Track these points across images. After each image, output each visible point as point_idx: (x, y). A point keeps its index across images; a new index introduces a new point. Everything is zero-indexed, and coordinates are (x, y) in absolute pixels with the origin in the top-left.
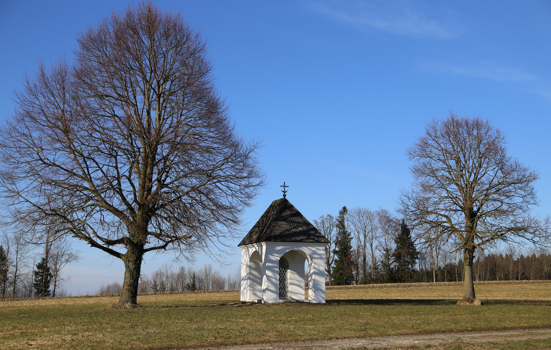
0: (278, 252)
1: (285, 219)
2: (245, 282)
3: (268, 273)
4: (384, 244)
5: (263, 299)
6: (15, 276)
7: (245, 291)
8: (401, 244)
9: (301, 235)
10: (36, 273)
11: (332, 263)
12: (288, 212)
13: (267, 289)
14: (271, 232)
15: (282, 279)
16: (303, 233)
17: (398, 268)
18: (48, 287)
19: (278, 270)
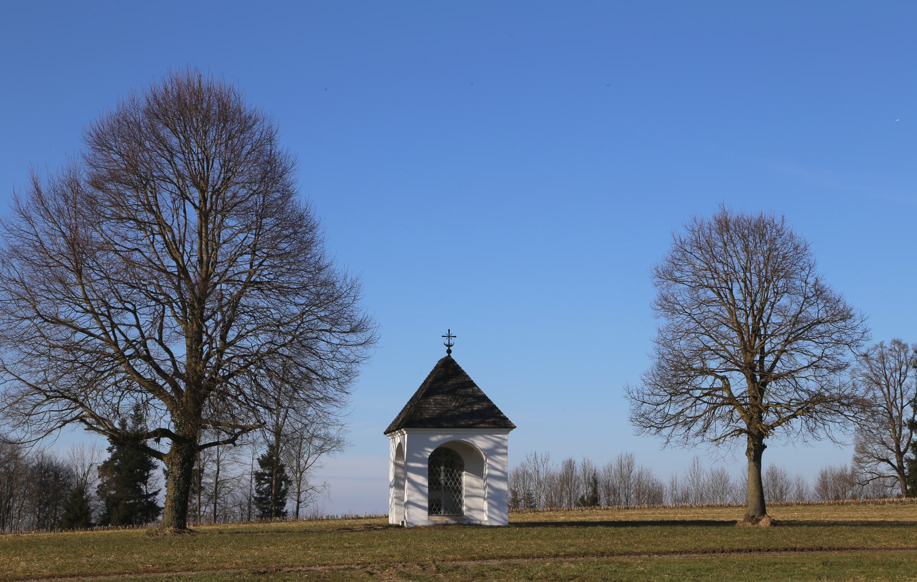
6: (217, 483)
10: (259, 477)
11: (905, 451)
18: (284, 504)
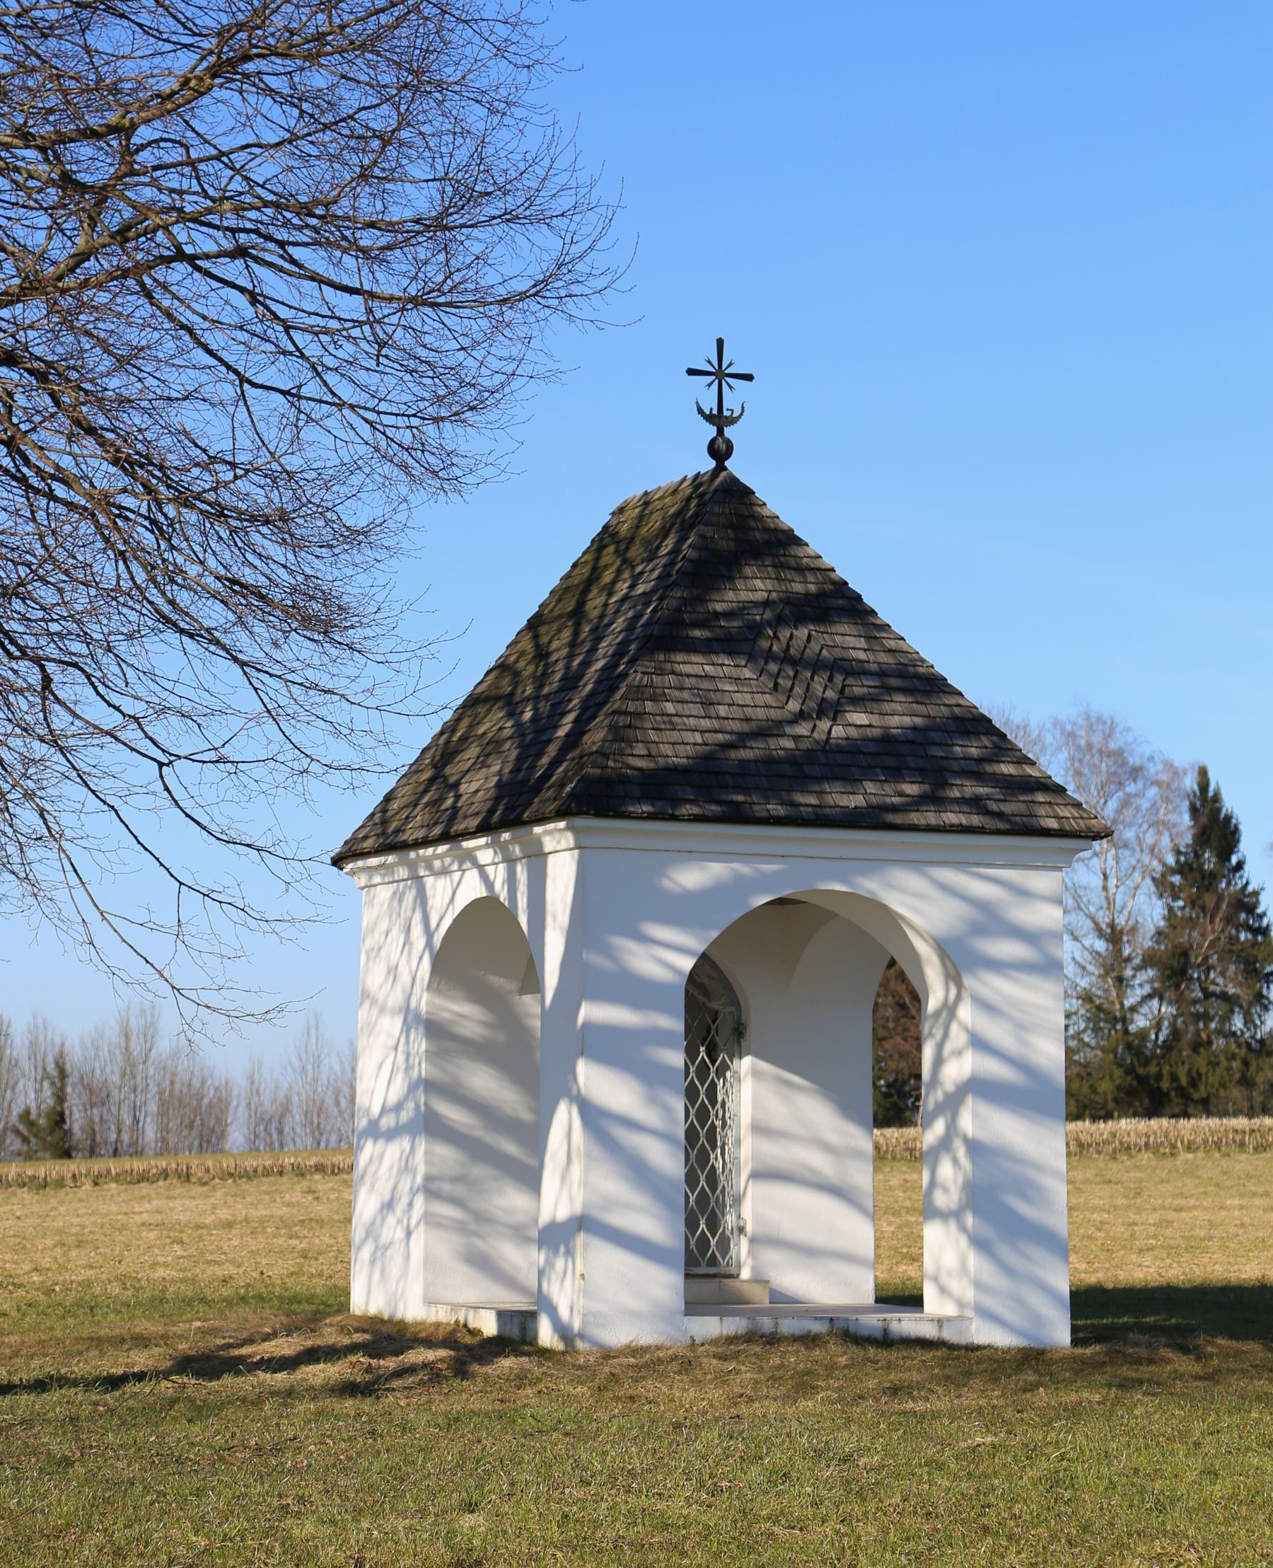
0: (680, 910)
1: (739, 640)
2: (394, 1151)
3: (597, 1081)
4: (1097, 898)
5: (544, 1303)
7: (392, 1230)
8: (1193, 903)
9: (868, 772)
12: (755, 586)
13: (583, 1223)
14: (619, 735)
15: (702, 1137)
16: (886, 756)
17: (1176, 1034)
19: (676, 1058)
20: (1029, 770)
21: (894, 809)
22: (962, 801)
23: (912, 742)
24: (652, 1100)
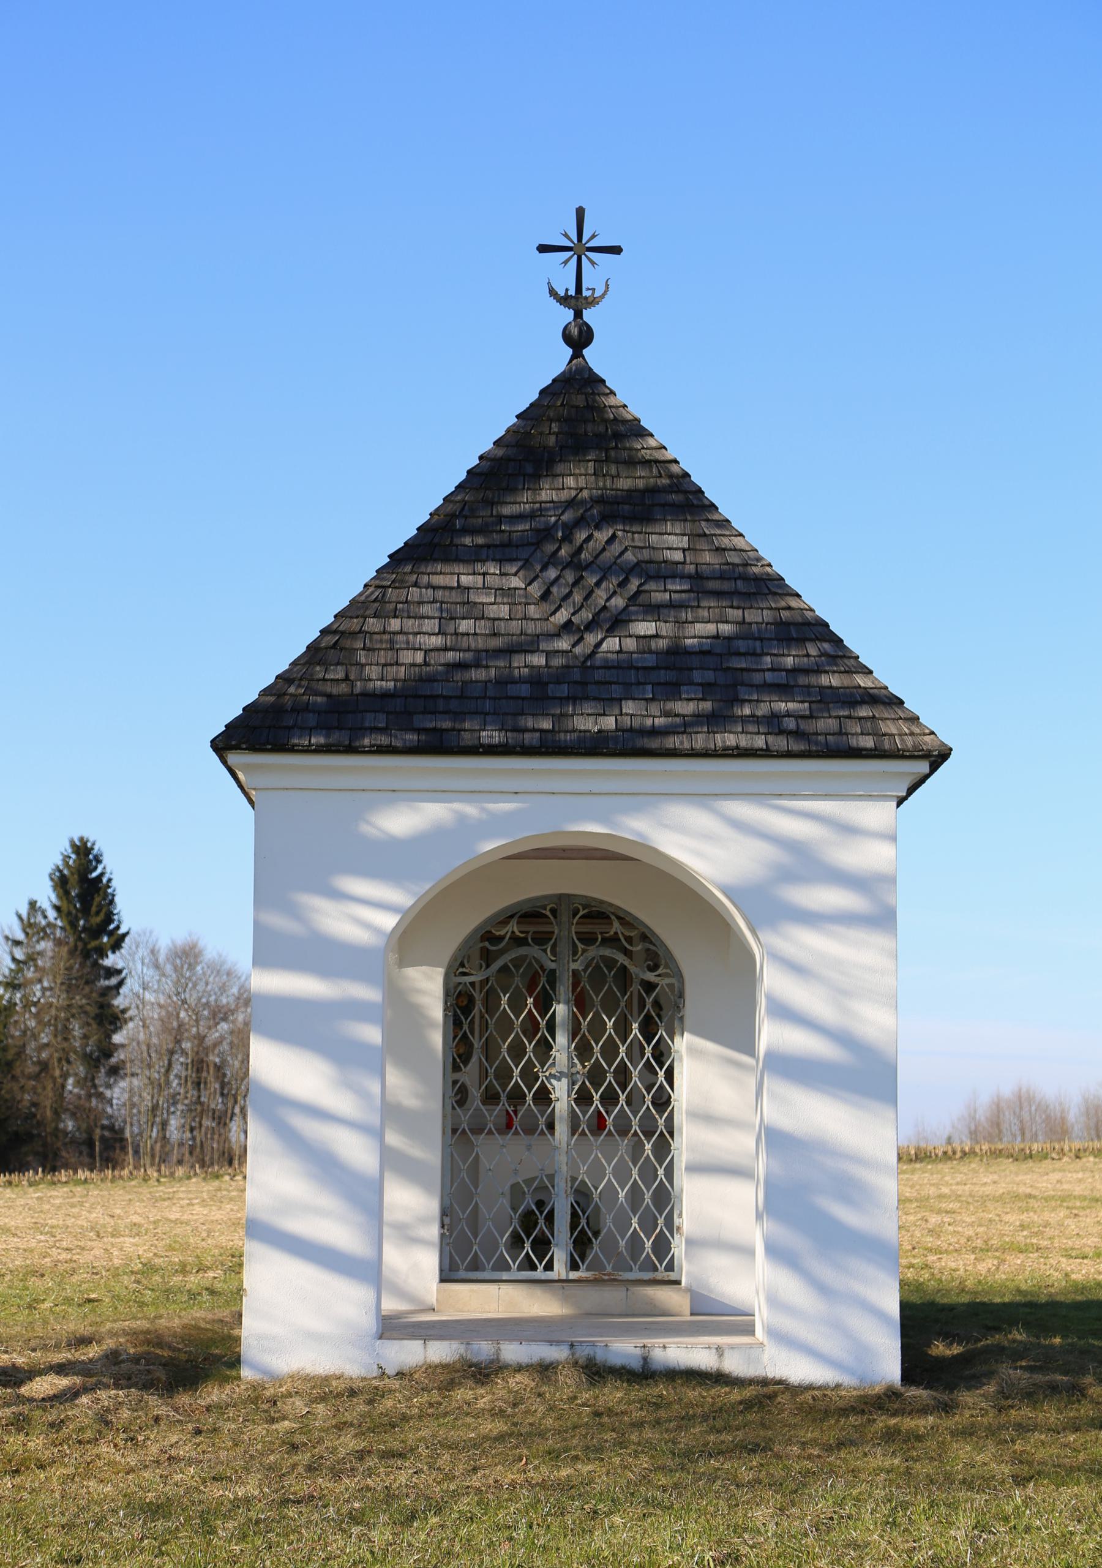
0: (386, 860)
16: (670, 671)
20: (861, 681)
21: (654, 732)
22: (754, 719)
23: (708, 653)
24: (348, 1085)
